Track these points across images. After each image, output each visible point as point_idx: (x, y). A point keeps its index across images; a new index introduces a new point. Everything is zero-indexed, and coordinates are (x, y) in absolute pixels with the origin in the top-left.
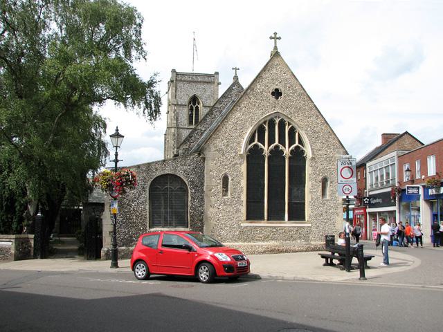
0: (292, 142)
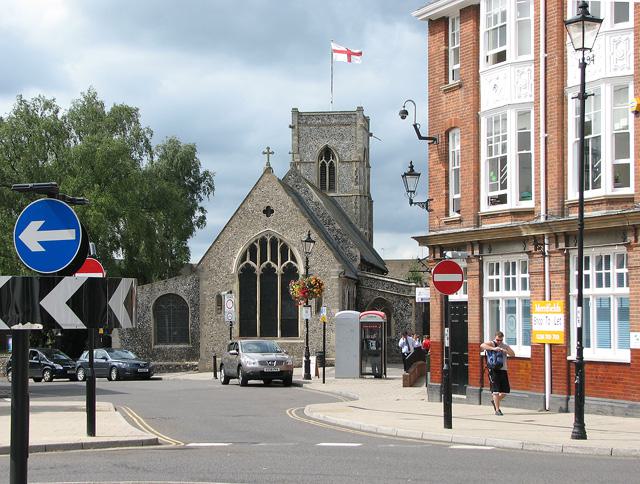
0: (284, 259)
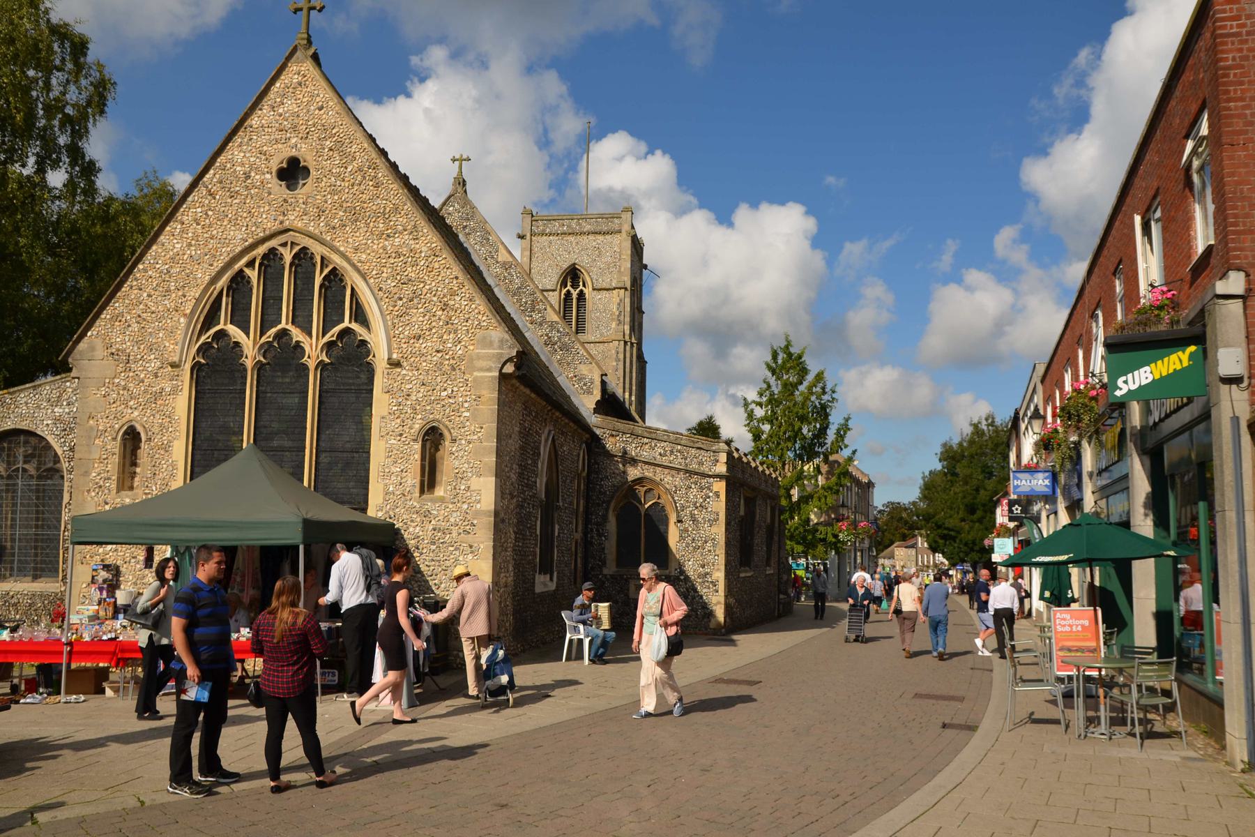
0: (332, 314)
